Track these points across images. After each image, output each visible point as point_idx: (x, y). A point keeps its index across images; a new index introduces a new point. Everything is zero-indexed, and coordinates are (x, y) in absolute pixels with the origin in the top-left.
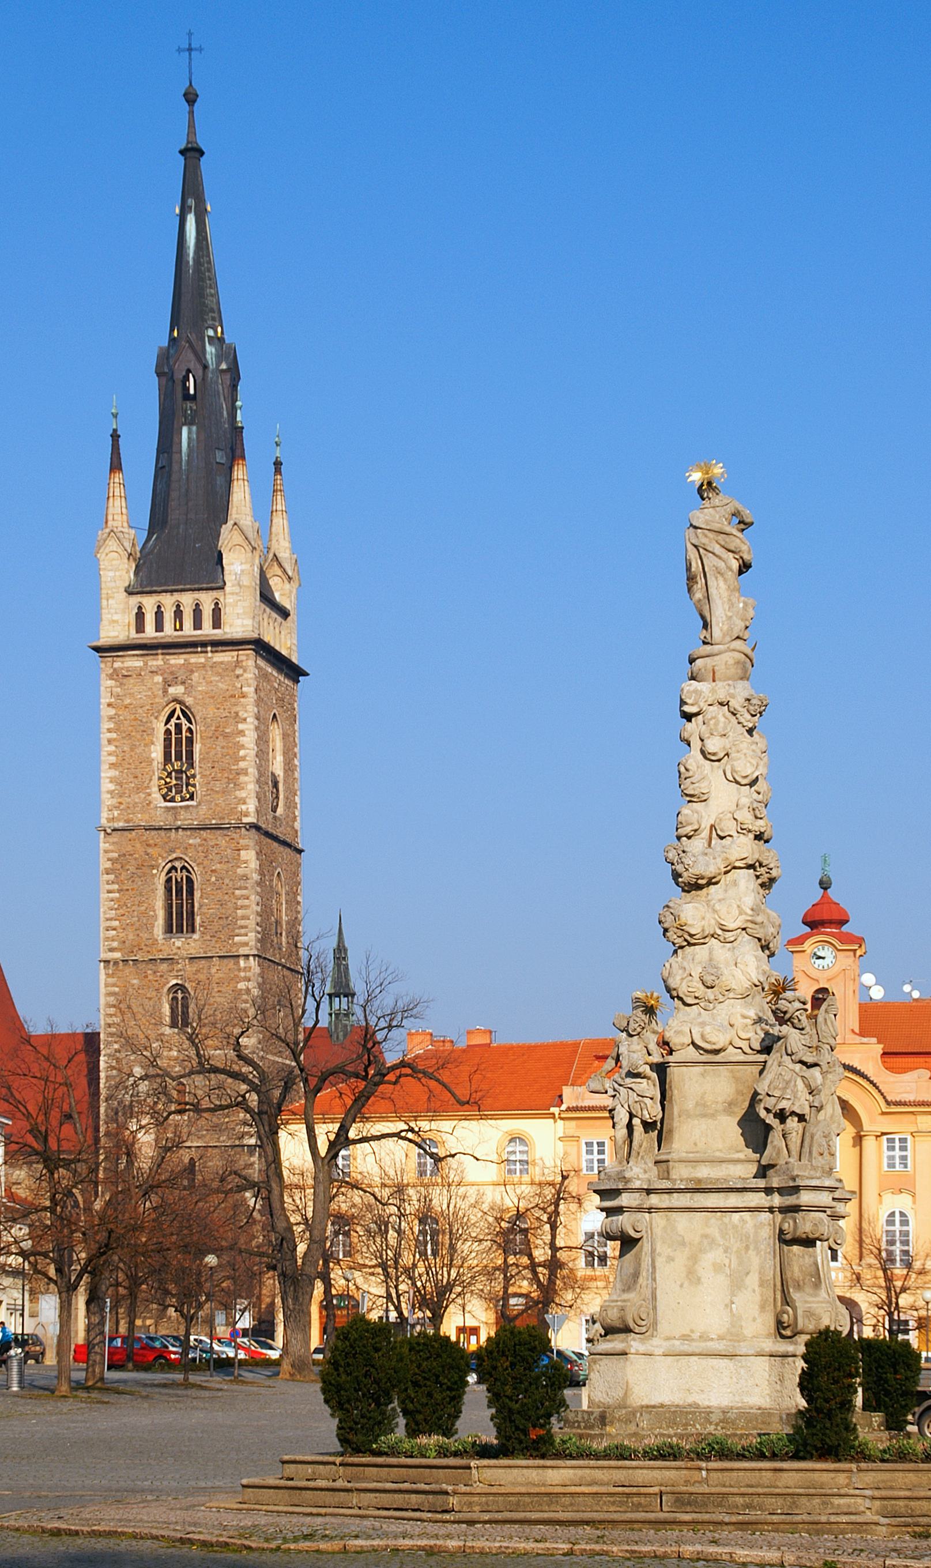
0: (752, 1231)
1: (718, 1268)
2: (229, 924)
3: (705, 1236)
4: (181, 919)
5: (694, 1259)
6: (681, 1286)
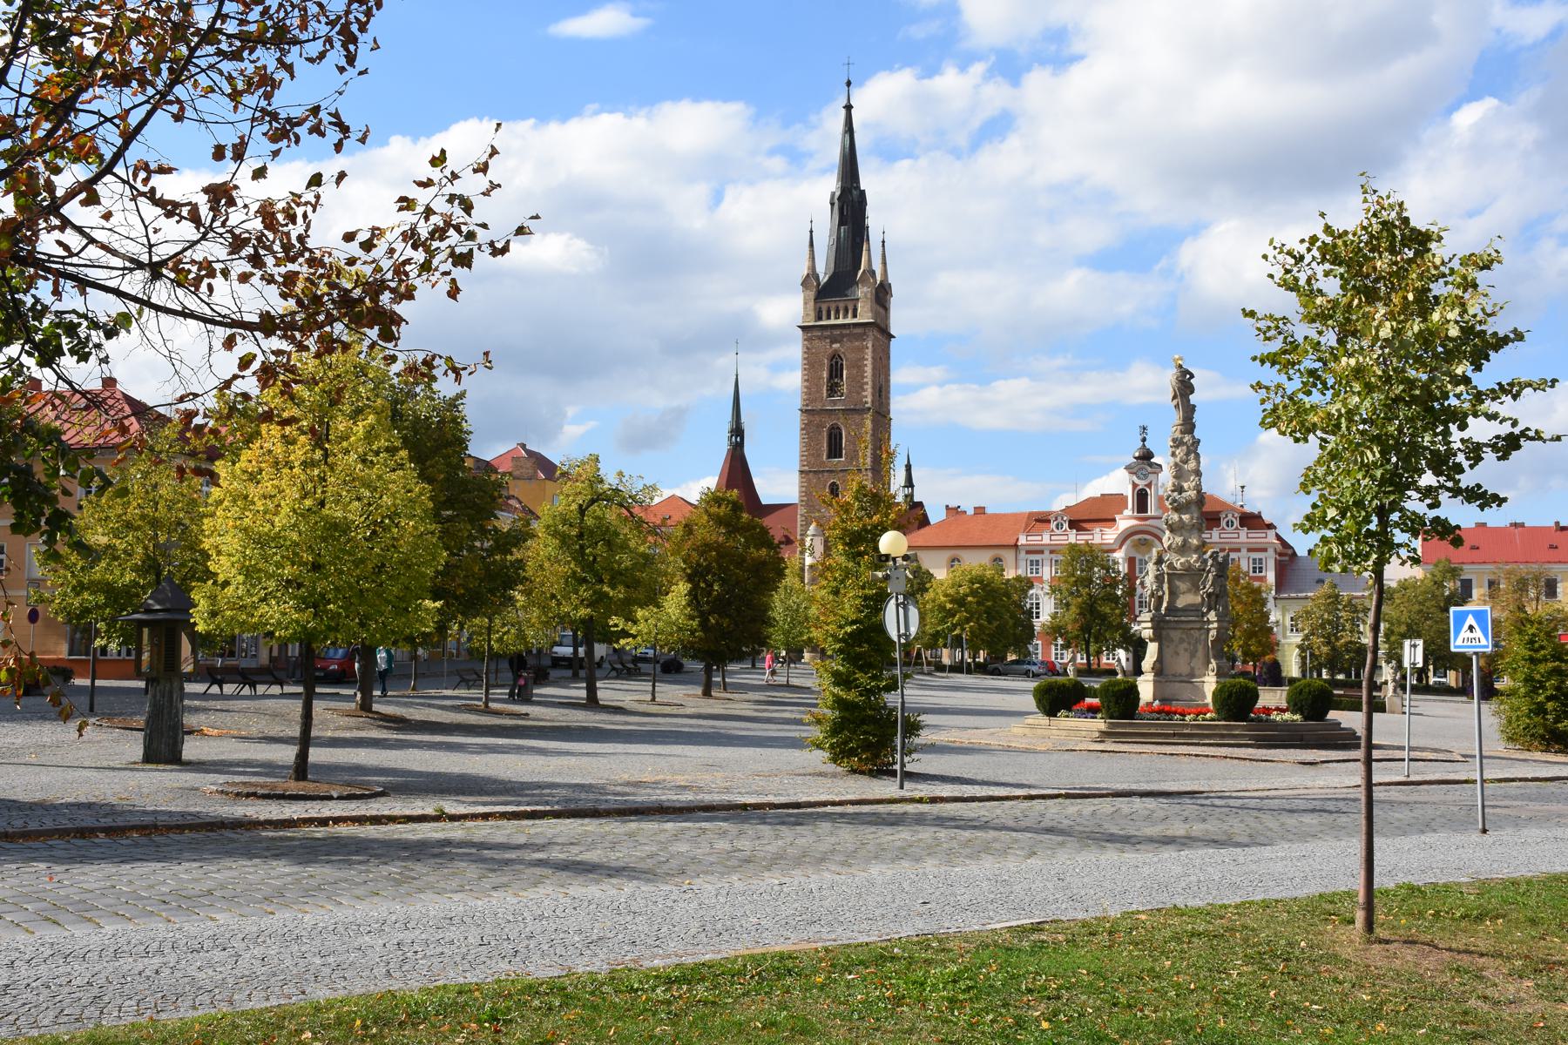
2: (854, 456)
4: (835, 450)
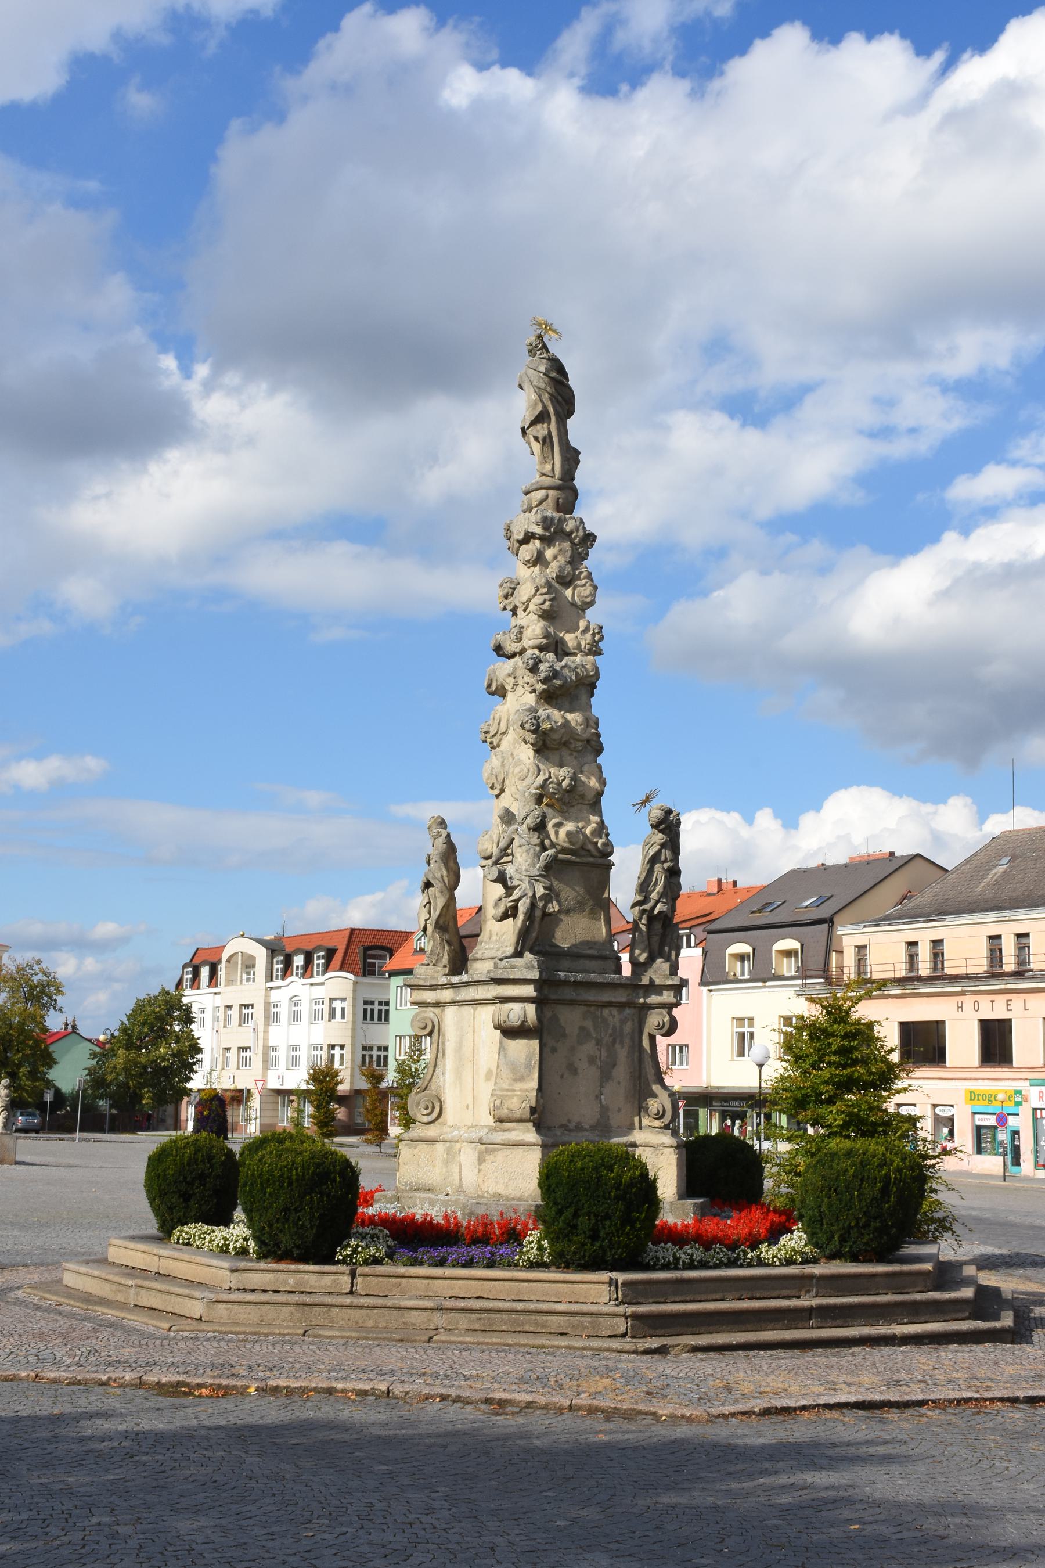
0: (618, 1025)
1: (592, 1060)
3: (582, 1029)
5: (573, 1049)
6: (562, 1076)
